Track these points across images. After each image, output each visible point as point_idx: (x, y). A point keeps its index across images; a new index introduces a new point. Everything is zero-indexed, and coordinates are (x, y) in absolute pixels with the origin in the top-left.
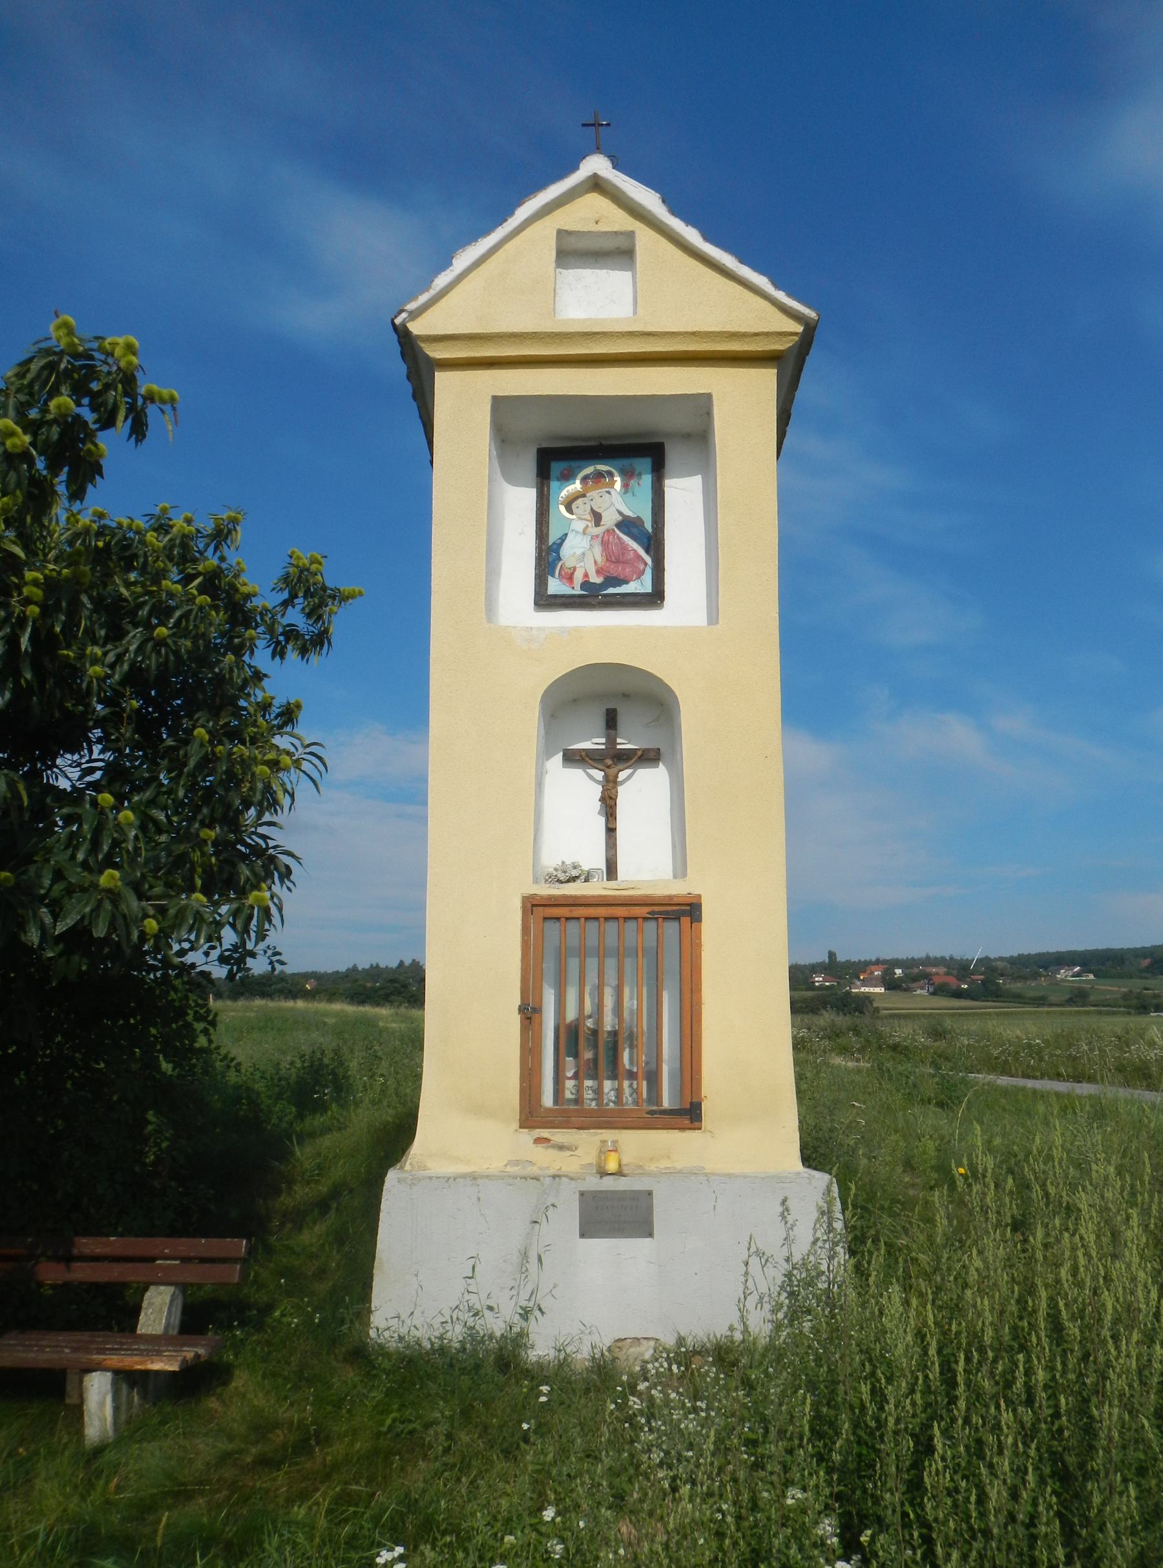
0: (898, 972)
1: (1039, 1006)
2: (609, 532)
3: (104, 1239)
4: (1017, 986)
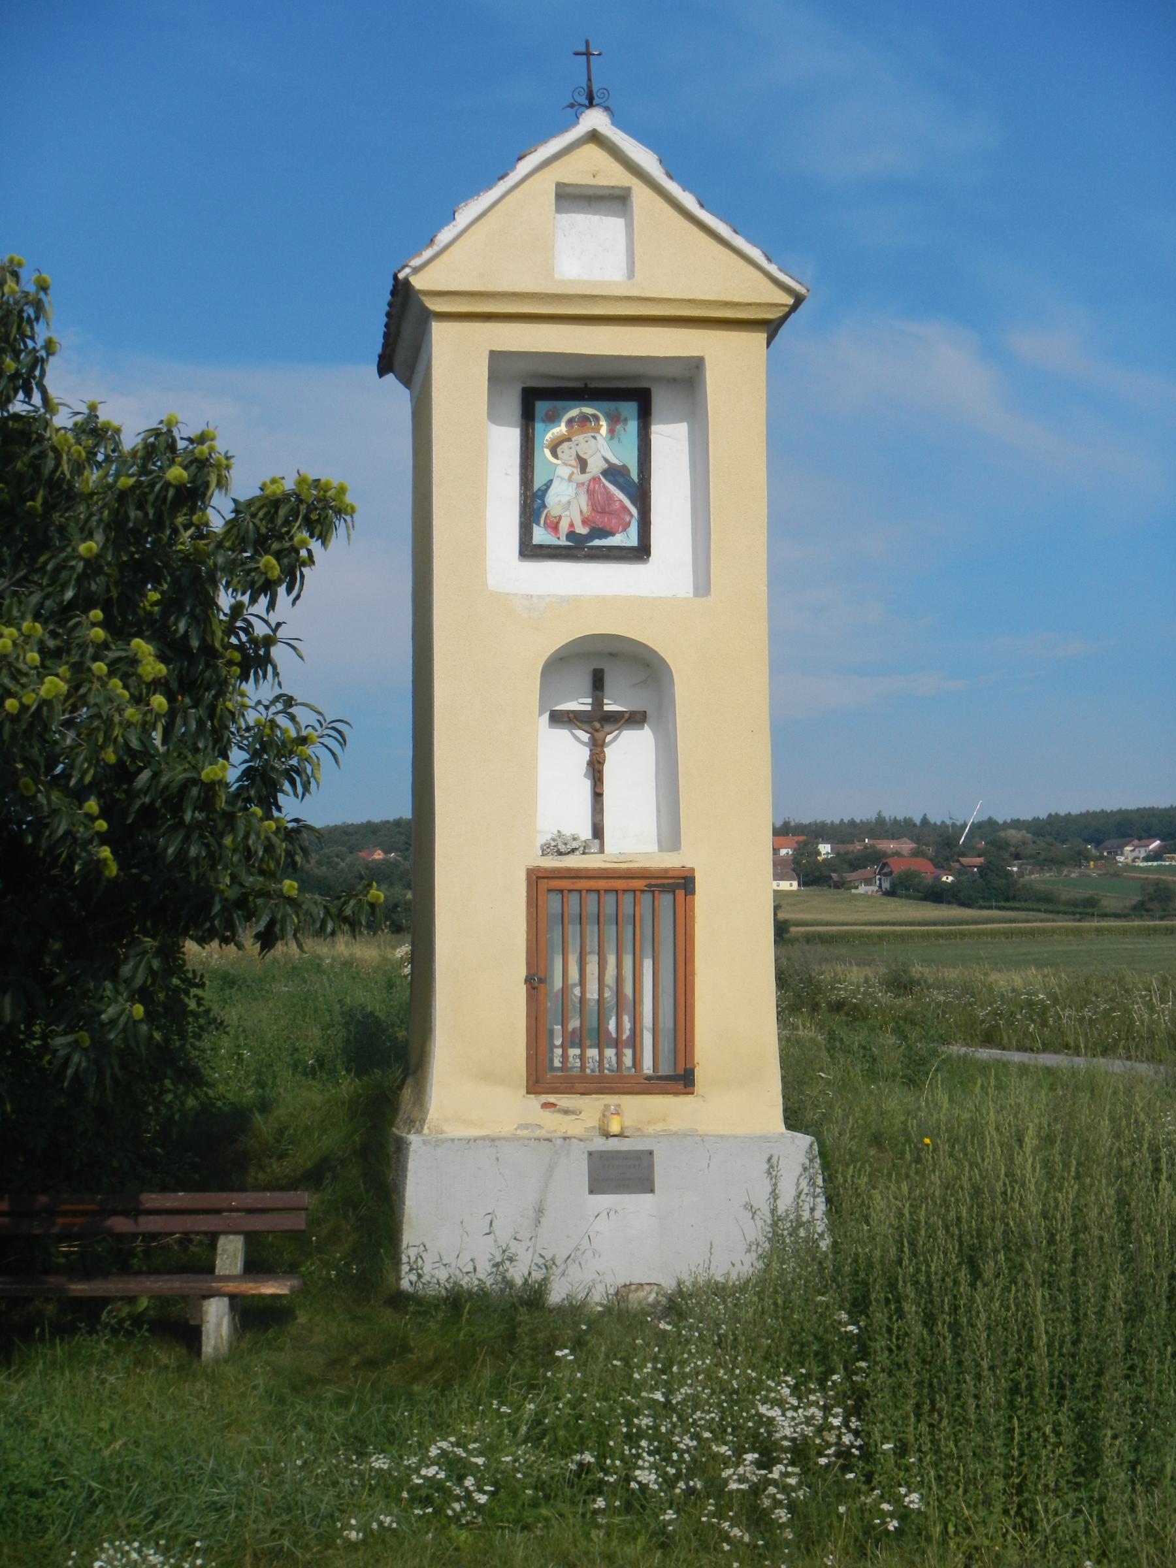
0: (825, 849)
1: (1083, 916)
2: (595, 480)
3: (172, 1195)
4: (1037, 878)
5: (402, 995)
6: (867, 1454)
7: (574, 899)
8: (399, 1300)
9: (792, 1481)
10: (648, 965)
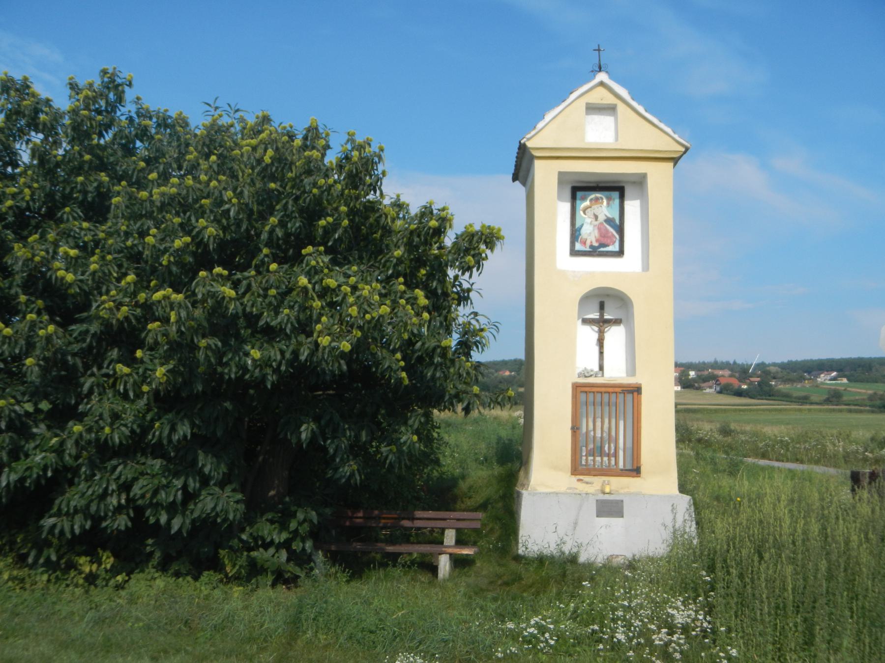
0: (692, 374)
1: (803, 404)
2: (601, 224)
4: (782, 387)
5: (519, 432)
6: (714, 631)
7: (591, 396)
8: (518, 558)
9: (682, 641)
10: (621, 423)
